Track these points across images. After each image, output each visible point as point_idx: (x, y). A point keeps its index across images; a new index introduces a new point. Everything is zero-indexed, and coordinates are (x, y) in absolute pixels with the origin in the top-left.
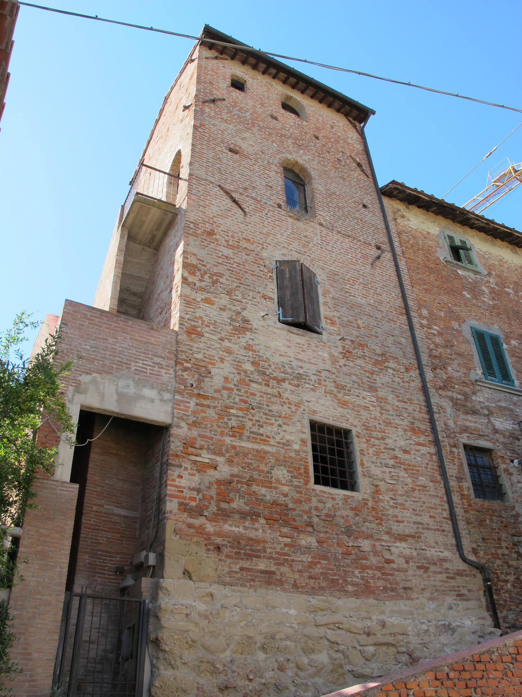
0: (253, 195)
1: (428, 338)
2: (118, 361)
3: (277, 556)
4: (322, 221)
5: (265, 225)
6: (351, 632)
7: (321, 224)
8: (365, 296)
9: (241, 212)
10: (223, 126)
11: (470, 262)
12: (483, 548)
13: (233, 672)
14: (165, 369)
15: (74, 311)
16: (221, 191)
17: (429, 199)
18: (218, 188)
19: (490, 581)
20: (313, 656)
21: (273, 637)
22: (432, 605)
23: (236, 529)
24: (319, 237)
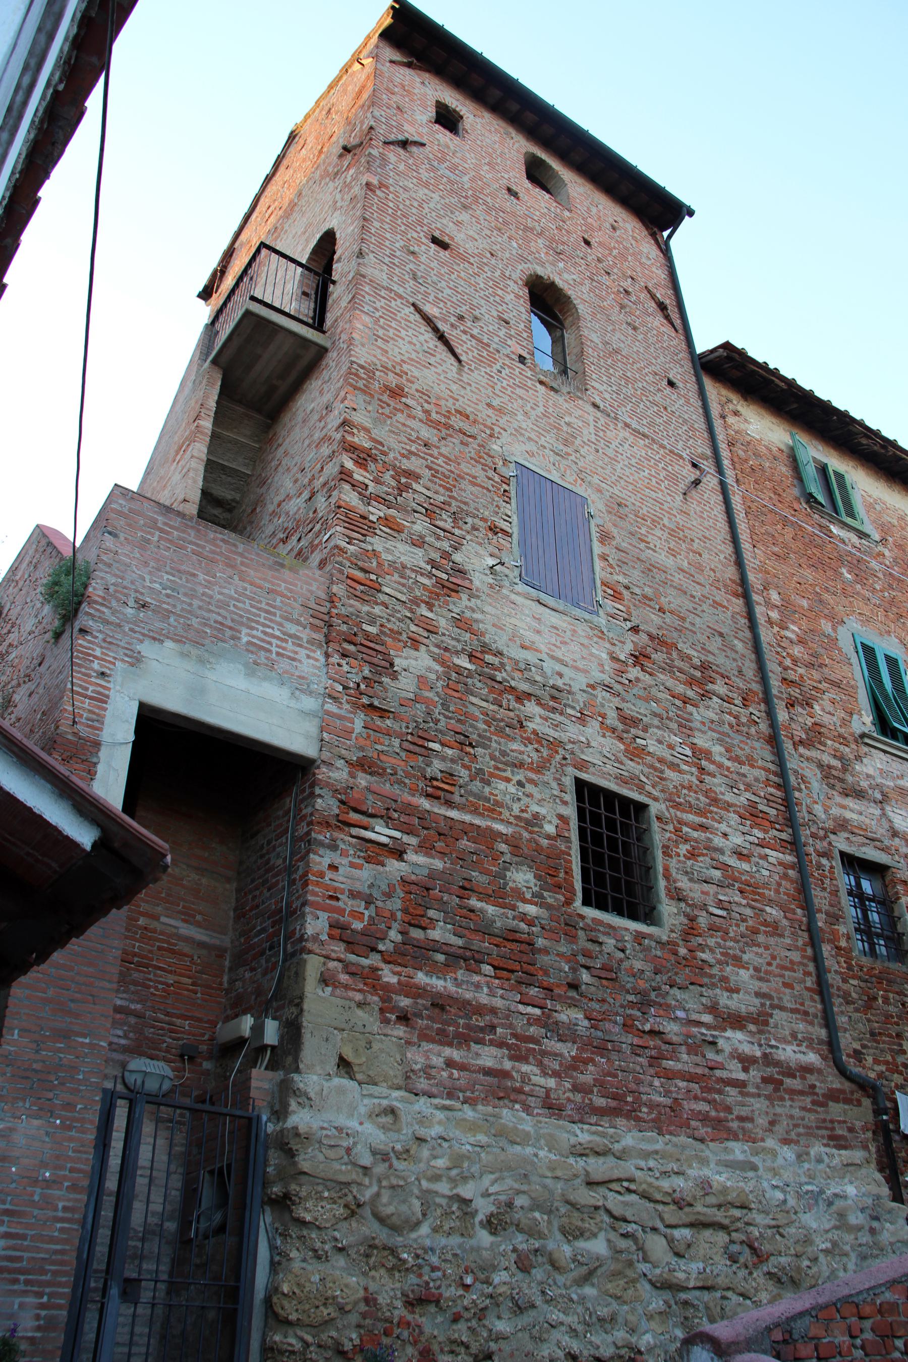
0: (475, 332)
1: (780, 646)
2: (216, 622)
3: (514, 1041)
4: (598, 401)
5: (497, 392)
6: (650, 1200)
7: (595, 406)
8: (673, 552)
9: (452, 360)
10: (422, 193)
11: (851, 514)
12: (872, 1051)
13: (434, 1269)
14: (306, 648)
15: (131, 510)
16: (418, 316)
17: (785, 387)
18: (412, 309)
19: (886, 1114)
20: (581, 1244)
21: (510, 1205)
22: (788, 1153)
23: (441, 983)
24: (592, 431)
